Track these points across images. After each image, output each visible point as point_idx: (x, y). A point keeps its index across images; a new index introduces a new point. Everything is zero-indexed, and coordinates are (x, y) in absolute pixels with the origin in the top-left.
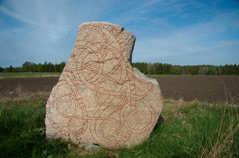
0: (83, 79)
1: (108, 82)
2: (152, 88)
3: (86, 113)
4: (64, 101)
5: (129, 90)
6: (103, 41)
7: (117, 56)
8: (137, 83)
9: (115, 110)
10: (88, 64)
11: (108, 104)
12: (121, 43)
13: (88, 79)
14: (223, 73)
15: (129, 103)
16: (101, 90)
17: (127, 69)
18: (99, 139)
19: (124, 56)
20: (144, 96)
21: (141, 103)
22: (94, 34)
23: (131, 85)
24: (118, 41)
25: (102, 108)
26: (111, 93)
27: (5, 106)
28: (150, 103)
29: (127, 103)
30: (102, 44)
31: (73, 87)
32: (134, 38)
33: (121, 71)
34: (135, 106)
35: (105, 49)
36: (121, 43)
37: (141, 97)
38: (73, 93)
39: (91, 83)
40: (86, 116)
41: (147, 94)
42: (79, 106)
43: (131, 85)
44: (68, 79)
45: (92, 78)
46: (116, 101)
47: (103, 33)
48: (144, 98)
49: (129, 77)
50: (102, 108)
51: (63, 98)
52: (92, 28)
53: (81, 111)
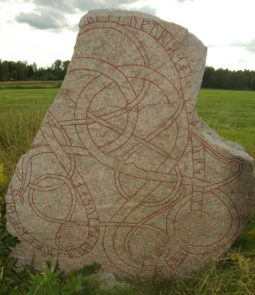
0: (88, 144)
3: (95, 213)
4: (47, 189)
6: (140, 62)
15: (188, 197)
16: (129, 169)
17: (191, 126)
19: (186, 98)
31: (66, 161)
33: (176, 130)
34: (201, 202)
39: (108, 154)
40: (95, 220)
43: (197, 161)
44: (53, 144)
45: (109, 143)
46: (161, 193)
47: (141, 43)
51: (43, 183)
53: (84, 211)
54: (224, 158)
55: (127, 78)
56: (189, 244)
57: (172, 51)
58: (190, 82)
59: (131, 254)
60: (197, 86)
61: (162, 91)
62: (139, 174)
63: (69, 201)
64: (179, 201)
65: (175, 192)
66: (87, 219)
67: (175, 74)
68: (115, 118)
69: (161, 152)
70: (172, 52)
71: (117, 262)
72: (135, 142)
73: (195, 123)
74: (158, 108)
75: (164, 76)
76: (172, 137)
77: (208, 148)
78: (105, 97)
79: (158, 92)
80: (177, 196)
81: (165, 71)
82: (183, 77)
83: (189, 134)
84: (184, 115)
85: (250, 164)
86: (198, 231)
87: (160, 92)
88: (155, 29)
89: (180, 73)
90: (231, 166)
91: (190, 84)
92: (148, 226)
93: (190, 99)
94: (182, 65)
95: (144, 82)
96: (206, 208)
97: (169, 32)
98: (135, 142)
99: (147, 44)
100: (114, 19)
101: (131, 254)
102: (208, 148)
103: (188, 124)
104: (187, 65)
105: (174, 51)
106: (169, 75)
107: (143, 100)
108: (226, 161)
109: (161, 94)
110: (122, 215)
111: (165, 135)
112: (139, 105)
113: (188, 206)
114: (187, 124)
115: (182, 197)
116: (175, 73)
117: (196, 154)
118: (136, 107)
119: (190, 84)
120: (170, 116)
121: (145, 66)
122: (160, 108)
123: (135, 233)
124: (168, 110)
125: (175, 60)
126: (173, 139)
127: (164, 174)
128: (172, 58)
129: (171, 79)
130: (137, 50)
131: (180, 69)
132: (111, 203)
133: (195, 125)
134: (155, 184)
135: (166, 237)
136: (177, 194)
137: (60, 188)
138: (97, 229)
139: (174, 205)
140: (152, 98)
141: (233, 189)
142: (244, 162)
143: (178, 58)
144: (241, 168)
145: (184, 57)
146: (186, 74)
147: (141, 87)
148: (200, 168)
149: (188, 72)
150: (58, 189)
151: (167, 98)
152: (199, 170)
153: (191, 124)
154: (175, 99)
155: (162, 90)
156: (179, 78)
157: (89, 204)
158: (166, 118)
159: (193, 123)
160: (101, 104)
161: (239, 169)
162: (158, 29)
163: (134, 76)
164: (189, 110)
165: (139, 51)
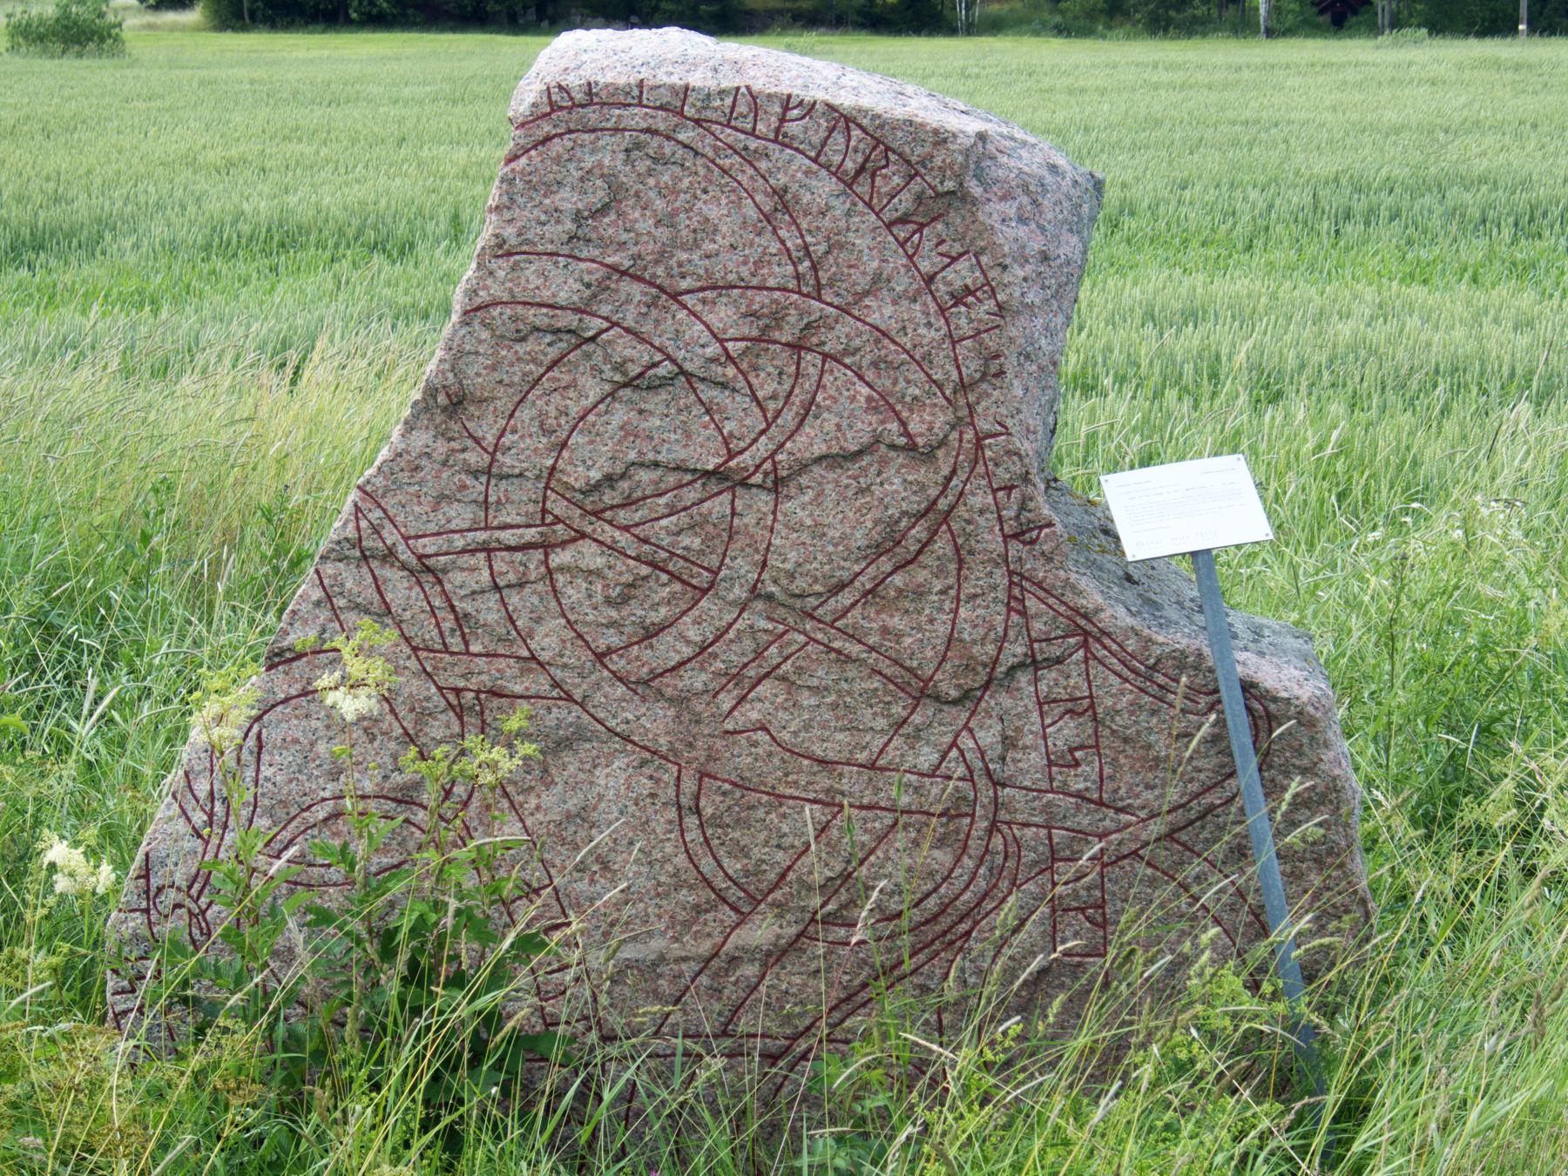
5: (1036, 758)
7: (914, 427)
12: (960, 297)
19: (984, 425)
24: (930, 279)
32: (743, 90)
33: (953, 567)
43: (1058, 710)
45: (650, 633)
49: (1038, 626)
57: (915, 227)
58: (997, 357)
65: (968, 863)
67: (929, 325)
70: (914, 233)
76: (935, 598)
81: (888, 310)
83: (1011, 583)
84: (980, 499)
94: (958, 284)
97: (894, 152)
102: (1105, 647)
103: (1005, 537)
105: (922, 226)
107: (797, 438)
109: (875, 408)
120: (919, 503)
121: (799, 293)
124: (910, 478)
139: (968, 933)
143: (941, 254)
145: (966, 252)
146: (980, 321)
148: (1077, 741)
151: (903, 424)
152: (1072, 750)
153: (1015, 536)
159: (1023, 533)
162: (849, 141)
163: (755, 333)
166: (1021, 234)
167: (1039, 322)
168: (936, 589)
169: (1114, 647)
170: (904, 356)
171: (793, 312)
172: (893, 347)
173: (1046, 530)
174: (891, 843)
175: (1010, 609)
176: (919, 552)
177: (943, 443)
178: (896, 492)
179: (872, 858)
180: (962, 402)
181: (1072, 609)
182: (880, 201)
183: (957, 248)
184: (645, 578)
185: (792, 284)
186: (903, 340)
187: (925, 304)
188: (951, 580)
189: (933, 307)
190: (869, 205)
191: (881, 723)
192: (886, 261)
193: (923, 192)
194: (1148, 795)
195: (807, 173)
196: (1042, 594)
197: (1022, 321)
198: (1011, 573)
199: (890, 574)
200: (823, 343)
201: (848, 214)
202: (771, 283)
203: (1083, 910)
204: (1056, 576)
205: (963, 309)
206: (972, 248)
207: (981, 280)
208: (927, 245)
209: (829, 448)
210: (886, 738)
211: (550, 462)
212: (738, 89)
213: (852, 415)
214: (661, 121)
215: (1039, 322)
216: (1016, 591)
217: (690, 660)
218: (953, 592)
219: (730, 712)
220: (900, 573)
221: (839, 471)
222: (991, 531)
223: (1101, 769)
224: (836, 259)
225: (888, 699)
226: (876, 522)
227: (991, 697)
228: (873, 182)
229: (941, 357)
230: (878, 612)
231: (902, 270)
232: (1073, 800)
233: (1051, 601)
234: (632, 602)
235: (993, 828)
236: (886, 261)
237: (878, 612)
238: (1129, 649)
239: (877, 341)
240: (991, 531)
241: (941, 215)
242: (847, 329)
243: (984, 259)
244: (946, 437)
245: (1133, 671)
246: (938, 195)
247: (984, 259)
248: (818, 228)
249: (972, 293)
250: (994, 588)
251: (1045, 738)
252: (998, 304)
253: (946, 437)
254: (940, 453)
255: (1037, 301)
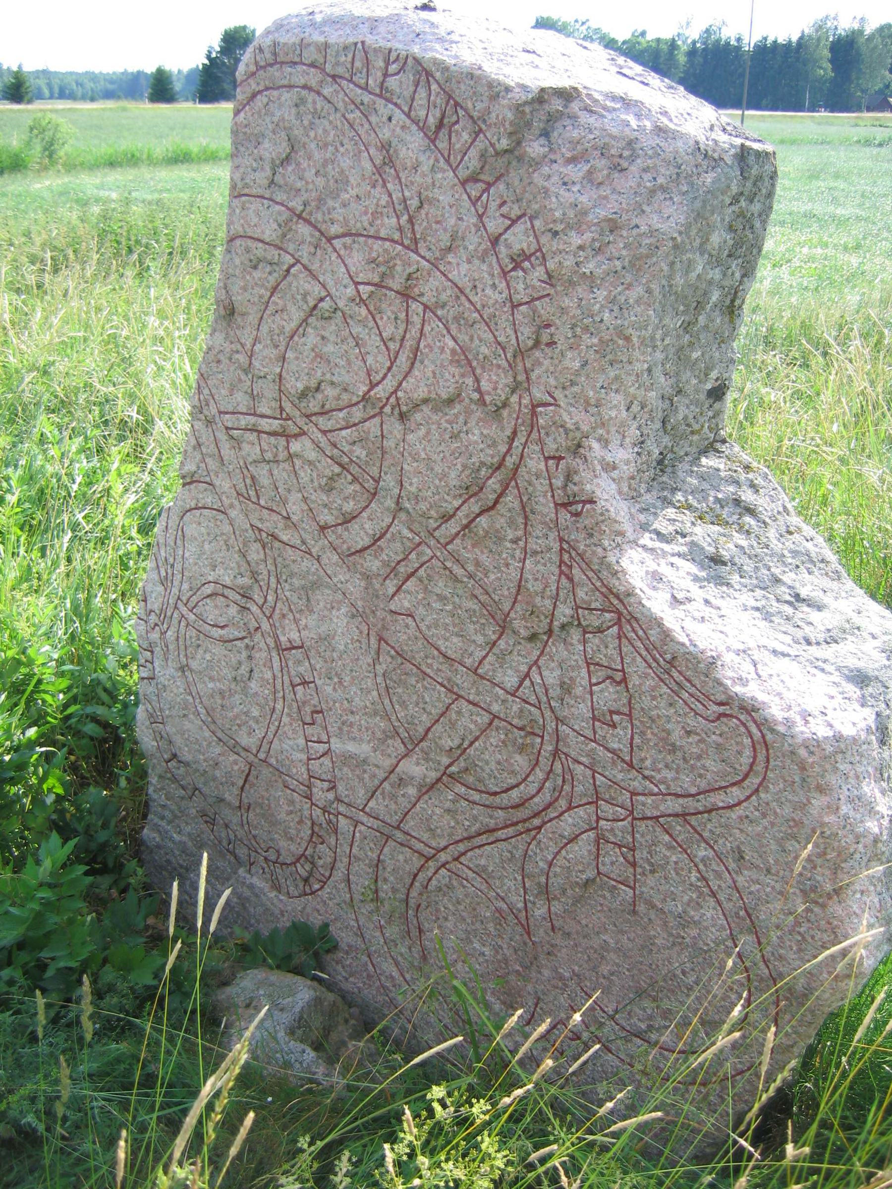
1: (441, 586)
2: (760, 767)
3: (326, 761)
4: (217, 633)
5: (584, 709)
6: (388, 224)
7: (485, 385)
8: (636, 668)
9: (492, 823)
10: (313, 406)
11: (446, 761)
12: (519, 261)
13: (326, 517)
14: (109, 95)
15: (581, 812)
17: (565, 516)
18: (395, 974)
19: (539, 394)
20: (691, 804)
21: (670, 848)
22: (326, 145)
23: (602, 674)
24: (495, 241)
25: (414, 768)
26: (463, 680)
27: (435, 602)
28: (741, 880)
29: (570, 808)
30: (377, 245)
32: (359, 46)
33: (521, 520)
35: (405, 295)
36: (517, 266)
37: (672, 805)
38: (256, 588)
40: (326, 785)
41: (719, 799)
42: (290, 696)
43: (602, 674)
45: (348, 519)
47: (385, 147)
48: (693, 820)
49: (581, 594)
50: (414, 768)
52: (313, 83)
53: (301, 741)
54: (692, 690)
55: (357, 284)
56: (601, 1009)
57: (484, 186)
58: (548, 326)
59: (424, 958)
60: (595, 341)
61: (459, 351)
62: (429, 661)
63: (267, 692)
64: (553, 815)
65: (539, 774)
66: (305, 776)
67: (494, 286)
68: (349, 431)
69: (483, 598)
70: (484, 191)
71: (385, 966)
72: (410, 535)
73: (579, 507)
74: (456, 416)
75: (462, 292)
76: (509, 545)
77: (634, 630)
78: (316, 346)
79: (448, 354)
80: (546, 796)
81: (464, 267)
82: (524, 300)
83: (562, 549)
84: (534, 463)
85: (792, 753)
86: (628, 970)
87: (453, 352)
88: (422, 93)
89: (513, 284)
90: (721, 735)
91: (552, 335)
92: (470, 873)
93: (552, 401)
94: (517, 247)
95: (408, 307)
96: (649, 885)
97: (462, 107)
98: (410, 535)
99: (403, 153)
100: (310, 55)
101: (424, 958)
102: (634, 630)
103: (556, 505)
104: (533, 250)
105: (489, 185)
106: (475, 287)
107: (409, 379)
108: (701, 707)
109: (458, 361)
110: (393, 797)
111: (487, 532)
112: (400, 394)
113: (582, 848)
114: (552, 505)
115: (563, 803)
116: (497, 282)
117: (597, 641)
118: (392, 400)
119: (552, 335)
120: (492, 457)
121: (402, 244)
122: (461, 419)
123: (434, 882)
124: (485, 432)
125: (494, 225)
126: (513, 557)
127: (497, 689)
128: (509, 219)
129: (484, 306)
130: (377, 176)
131: (511, 266)
132: (369, 742)
133: (577, 514)
134: (474, 717)
135: (525, 944)
136: (547, 784)
137: (246, 641)
138: (330, 821)
139: (539, 828)
140: (434, 373)
141: (743, 843)
142: (769, 737)
143: (502, 215)
144: (761, 757)
145: (524, 215)
146: (533, 287)
147: (402, 327)
148: (614, 706)
149: (540, 280)
150: (238, 643)
151: (477, 380)
152: (611, 712)
153: (564, 505)
154: (499, 391)
155: (461, 348)
156: (508, 305)
157: (313, 724)
158: (483, 464)
159: (571, 504)
160: (306, 371)
161: (755, 757)
162: (430, 95)
163: (376, 280)
164: (551, 447)
165: (384, 181)
166: (584, 199)
167: (601, 294)
168: (509, 538)
169: (641, 633)
170: (476, 315)
171: (398, 262)
172: (467, 305)
173: (588, 506)
174: (488, 737)
175: (561, 572)
176: (496, 502)
177: (505, 405)
178: (476, 442)
179: (477, 744)
180: (520, 367)
181: (606, 587)
182: (455, 158)
183: (516, 212)
184: (338, 475)
185: (396, 236)
186: (475, 299)
187: (490, 265)
188: (520, 533)
189: (497, 271)
190: (447, 161)
191: (480, 639)
192: (461, 219)
193: (486, 150)
194: (669, 775)
195: (403, 128)
196: (584, 566)
197: (581, 290)
198: (561, 540)
199: (478, 515)
200: (422, 295)
201: (433, 169)
202: (383, 234)
203: (620, 846)
204: (594, 553)
205: (521, 273)
206: (529, 211)
207: (534, 246)
208: (493, 205)
209: (430, 392)
210: (484, 653)
211: (278, 370)
212: (356, 44)
213: (442, 366)
214: (313, 78)
215: (601, 294)
216: (566, 557)
217: (369, 547)
218: (521, 543)
219: (393, 596)
220: (486, 515)
221: (440, 414)
222: (545, 496)
223: (632, 738)
224: (427, 214)
225: (483, 621)
226: (465, 467)
227: (553, 644)
228: (450, 139)
229: (504, 320)
230: (474, 546)
231: (473, 230)
232: (610, 755)
233: (591, 574)
234: (334, 492)
235: (556, 753)
236: (461, 219)
237: (474, 546)
238: (652, 639)
239: (458, 297)
240: (545, 496)
241: (502, 175)
242: (437, 283)
243: (537, 223)
244: (507, 399)
245: (655, 660)
246: (497, 154)
247: (537, 223)
248: (412, 183)
249: (528, 258)
250: (549, 549)
251: (591, 694)
252: (547, 272)
253: (507, 399)
254: (505, 413)
255: (598, 272)
